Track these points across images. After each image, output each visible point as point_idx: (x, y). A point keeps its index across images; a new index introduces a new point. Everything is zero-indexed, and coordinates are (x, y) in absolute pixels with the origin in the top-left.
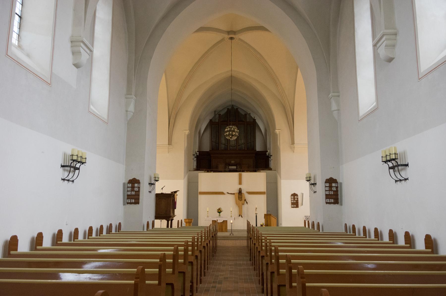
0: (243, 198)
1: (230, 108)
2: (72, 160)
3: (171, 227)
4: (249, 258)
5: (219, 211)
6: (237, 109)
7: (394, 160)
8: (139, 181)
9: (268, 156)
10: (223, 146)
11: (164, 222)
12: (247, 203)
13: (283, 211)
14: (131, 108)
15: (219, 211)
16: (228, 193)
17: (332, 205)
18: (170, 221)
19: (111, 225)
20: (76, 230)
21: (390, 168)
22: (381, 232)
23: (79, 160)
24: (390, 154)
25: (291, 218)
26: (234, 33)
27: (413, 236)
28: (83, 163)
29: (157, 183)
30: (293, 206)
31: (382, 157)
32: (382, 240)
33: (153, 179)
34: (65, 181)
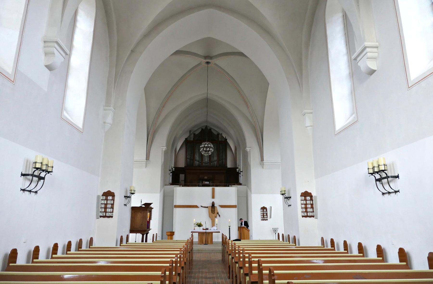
1: (204, 128)
2: (35, 168)
3: (146, 241)
4: (226, 275)
6: (210, 129)
7: (383, 171)
8: (113, 193)
9: (238, 172)
11: (139, 236)
12: (219, 215)
13: (253, 223)
14: (109, 120)
16: (202, 206)
18: (145, 235)
19: (81, 240)
20: (37, 249)
21: (377, 180)
22: (350, 245)
23: (44, 168)
24: (379, 165)
25: (261, 232)
26: (211, 58)
27: (365, 247)
28: (49, 172)
29: (133, 196)
31: (368, 169)
32: (351, 253)
33: (129, 192)
34: (25, 192)
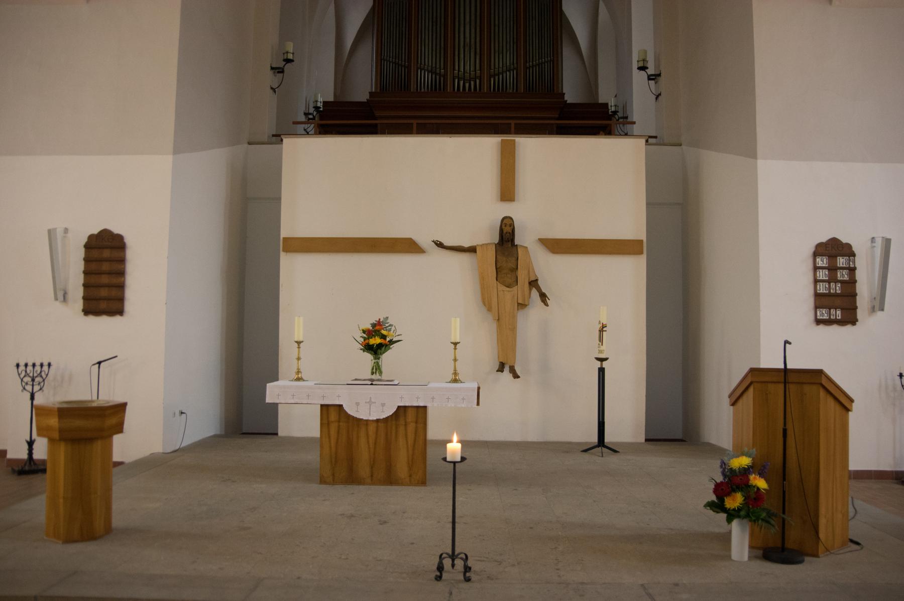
0: (522, 275)
5: (376, 342)
10: (426, 78)
12: (543, 296)
15: (376, 342)
16: (440, 245)
17: (835, 328)
30: (823, 314)
